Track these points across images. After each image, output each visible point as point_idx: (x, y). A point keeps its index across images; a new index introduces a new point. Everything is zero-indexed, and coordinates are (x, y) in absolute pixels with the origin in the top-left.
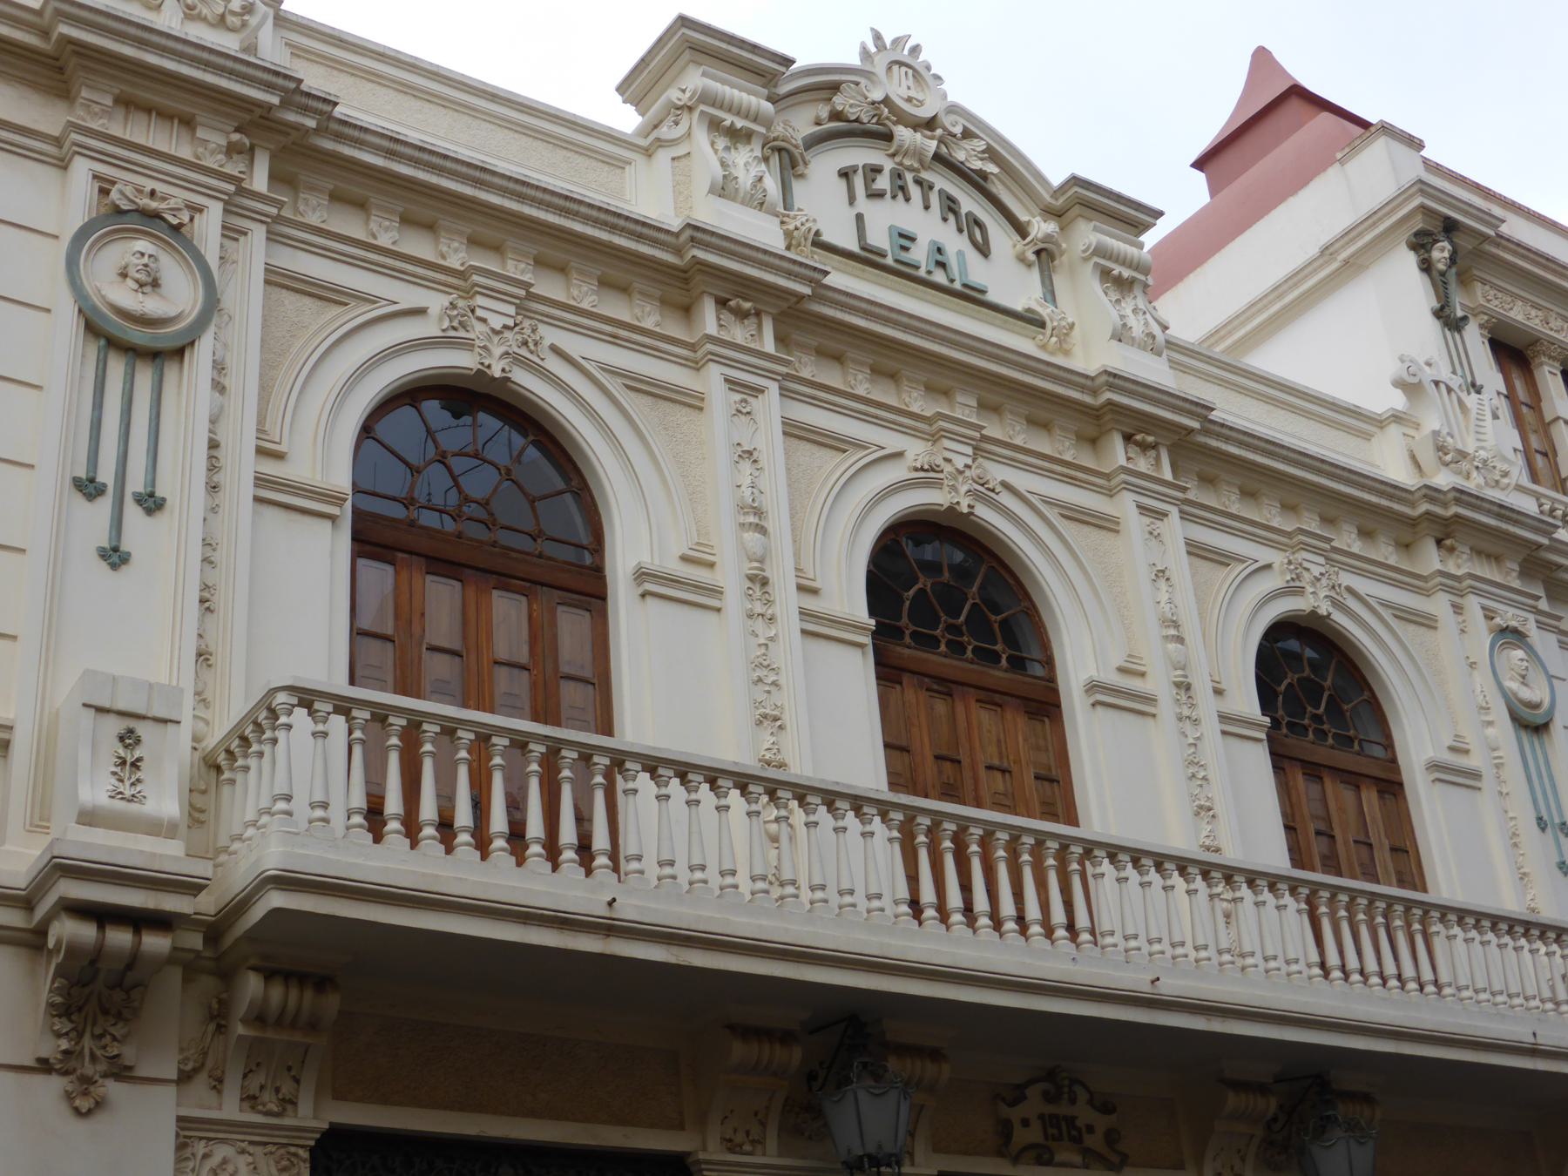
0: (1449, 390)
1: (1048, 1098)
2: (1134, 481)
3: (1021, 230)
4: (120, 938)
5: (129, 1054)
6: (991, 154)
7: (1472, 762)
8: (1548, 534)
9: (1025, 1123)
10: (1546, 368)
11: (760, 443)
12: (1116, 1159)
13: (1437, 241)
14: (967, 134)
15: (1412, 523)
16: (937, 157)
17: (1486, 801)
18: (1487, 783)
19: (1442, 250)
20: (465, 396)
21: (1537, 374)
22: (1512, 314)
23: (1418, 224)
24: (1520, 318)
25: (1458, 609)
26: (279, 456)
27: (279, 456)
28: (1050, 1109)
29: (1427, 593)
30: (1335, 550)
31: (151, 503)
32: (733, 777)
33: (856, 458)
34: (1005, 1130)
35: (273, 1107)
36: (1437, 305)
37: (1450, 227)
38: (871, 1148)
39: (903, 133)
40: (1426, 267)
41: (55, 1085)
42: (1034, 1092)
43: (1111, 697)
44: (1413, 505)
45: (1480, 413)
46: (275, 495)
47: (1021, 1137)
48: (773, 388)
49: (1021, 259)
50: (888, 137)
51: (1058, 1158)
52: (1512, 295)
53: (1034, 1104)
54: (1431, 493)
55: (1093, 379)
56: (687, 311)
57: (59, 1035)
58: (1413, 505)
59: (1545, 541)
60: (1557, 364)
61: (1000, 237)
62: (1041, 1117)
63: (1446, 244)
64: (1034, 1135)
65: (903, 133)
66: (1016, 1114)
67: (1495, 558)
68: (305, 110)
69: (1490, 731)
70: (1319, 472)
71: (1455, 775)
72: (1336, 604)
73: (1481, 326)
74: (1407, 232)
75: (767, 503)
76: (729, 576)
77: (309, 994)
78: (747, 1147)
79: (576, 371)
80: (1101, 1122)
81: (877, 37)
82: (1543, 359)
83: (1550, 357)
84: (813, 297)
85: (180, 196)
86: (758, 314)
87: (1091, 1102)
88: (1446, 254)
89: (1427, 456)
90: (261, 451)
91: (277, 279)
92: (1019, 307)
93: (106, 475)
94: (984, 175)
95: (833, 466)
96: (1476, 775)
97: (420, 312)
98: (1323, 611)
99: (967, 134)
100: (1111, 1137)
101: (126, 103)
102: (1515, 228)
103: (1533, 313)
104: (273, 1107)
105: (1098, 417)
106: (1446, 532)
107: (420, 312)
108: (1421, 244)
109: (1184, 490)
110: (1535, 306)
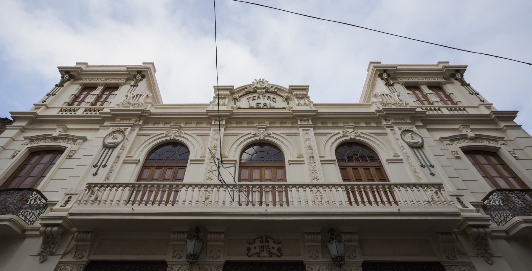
0: (387, 95)
1: (261, 242)
2: (302, 126)
3: (282, 97)
4: (481, 230)
5: (54, 251)
6: (276, 88)
7: (400, 158)
9: (255, 248)
11: (310, 137)
12: (279, 254)
14: (272, 87)
15: (378, 118)
16: (266, 92)
17: (405, 164)
20: (262, 143)
23: (378, 73)
25: (392, 130)
26: (324, 157)
27: (324, 157)
28: (261, 245)
29: (385, 129)
31: (433, 167)
32: (208, 189)
33: (330, 136)
34: (249, 249)
35: (352, 257)
37: (385, 71)
38: (340, 255)
39: (259, 91)
40: (382, 79)
42: (258, 241)
43: (292, 162)
45: (394, 97)
46: (323, 162)
47: (253, 251)
48: (312, 129)
49: (283, 101)
50: (257, 92)
51: (261, 255)
53: (258, 243)
56: (381, 123)
61: (278, 99)
62: (259, 246)
64: (257, 250)
65: (259, 91)
66: (252, 247)
68: (146, 113)
69: (404, 151)
72: (356, 136)
74: (377, 76)
75: (312, 146)
76: (306, 159)
77: (315, 236)
78: (453, 258)
79: (366, 135)
80: (276, 246)
81: (256, 80)
84: (149, 115)
85: (123, 128)
86: (308, 120)
87: (274, 242)
90: (320, 157)
91: (316, 134)
92: (281, 107)
93: (424, 164)
94: (276, 92)
95: (326, 138)
96: (401, 160)
97: (339, 133)
98: (353, 137)
99: (272, 87)
100: (279, 250)
101: (122, 119)
102: (398, 67)
104: (352, 257)
106: (386, 117)
107: (339, 133)
108: (380, 76)
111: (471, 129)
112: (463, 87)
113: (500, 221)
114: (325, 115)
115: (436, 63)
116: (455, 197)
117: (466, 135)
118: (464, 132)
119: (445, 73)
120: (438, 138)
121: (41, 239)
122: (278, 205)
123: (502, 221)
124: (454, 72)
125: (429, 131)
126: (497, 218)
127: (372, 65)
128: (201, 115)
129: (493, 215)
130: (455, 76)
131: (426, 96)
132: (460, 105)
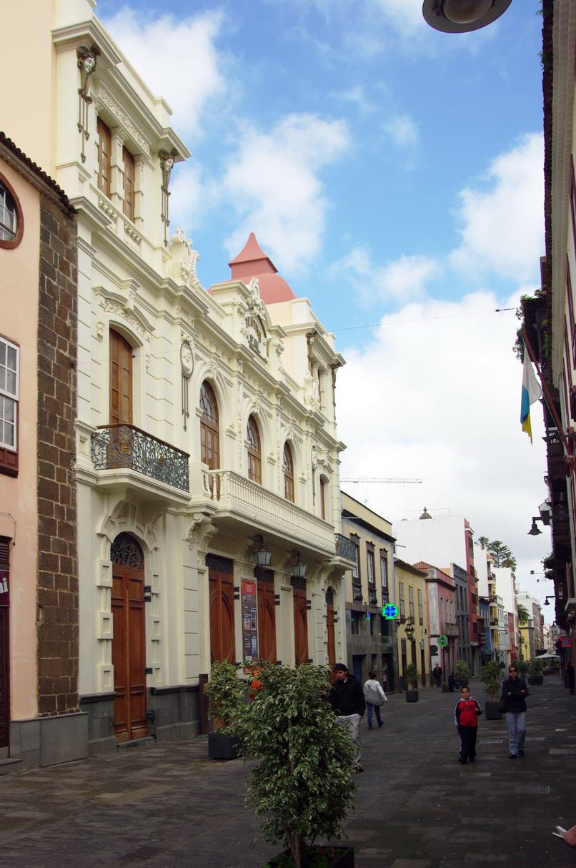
8: (252, 358)
10: (118, 141)
13: (169, 158)
15: (233, 353)
18: (237, 438)
19: (90, 62)
21: (113, 142)
22: (111, 109)
24: (114, 113)
30: (220, 361)
36: (80, 87)
40: (81, 66)
41: (188, 543)
44: (236, 348)
52: (114, 100)
54: (171, 282)
55: (162, 279)
57: (484, 636)
58: (236, 348)
59: (250, 360)
60: (122, 142)
63: (93, 60)
67: (187, 313)
70: (264, 374)
71: (231, 435)
73: (96, 108)
82: (118, 136)
83: (121, 137)
88: (91, 65)
89: (308, 400)
102: (120, 66)
103: (120, 113)
105: (158, 291)
109: (245, 377)
110: (121, 110)
111: (137, 295)
112: (161, 190)
113: (100, 462)
114: (126, 252)
115: (157, 95)
116: (298, 503)
117: (125, 300)
118: (125, 293)
119: (159, 140)
120: (97, 284)
121: (75, 467)
122: (214, 475)
123: (103, 464)
124: (169, 150)
125: (93, 265)
126: (99, 457)
127: (90, 24)
128: (219, 333)
129: (97, 452)
130: (165, 160)
131: (134, 193)
132: (138, 226)
